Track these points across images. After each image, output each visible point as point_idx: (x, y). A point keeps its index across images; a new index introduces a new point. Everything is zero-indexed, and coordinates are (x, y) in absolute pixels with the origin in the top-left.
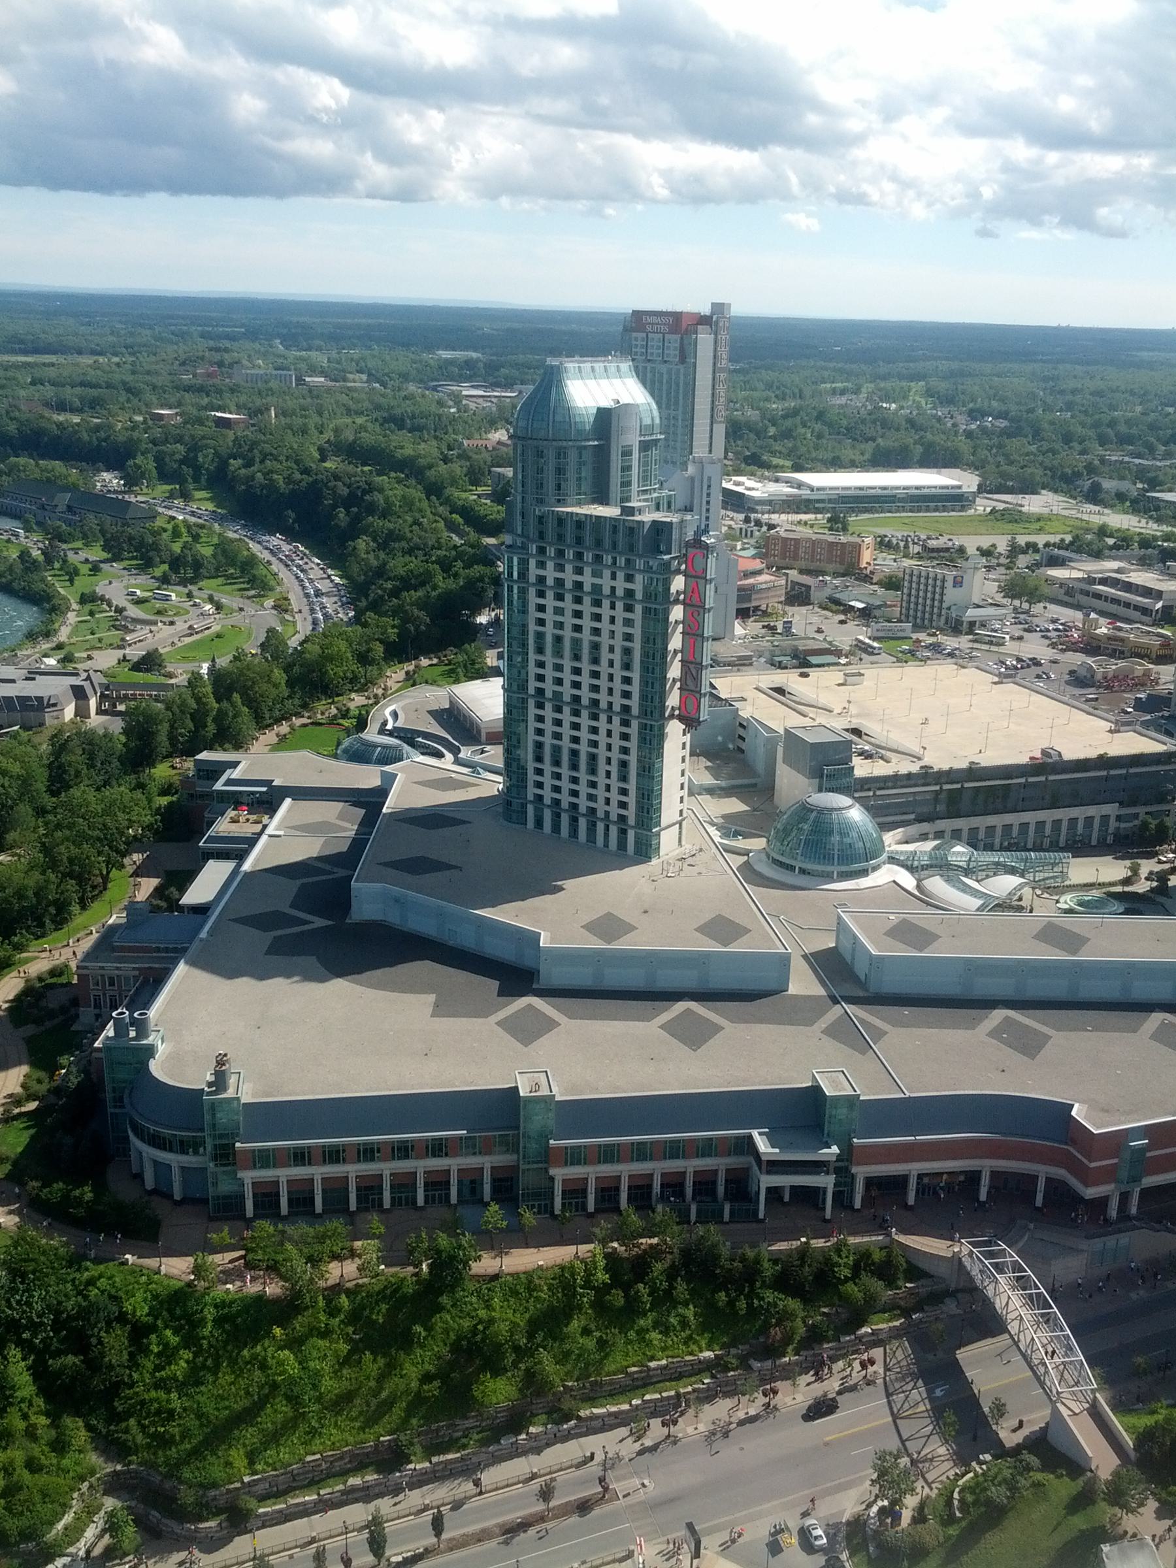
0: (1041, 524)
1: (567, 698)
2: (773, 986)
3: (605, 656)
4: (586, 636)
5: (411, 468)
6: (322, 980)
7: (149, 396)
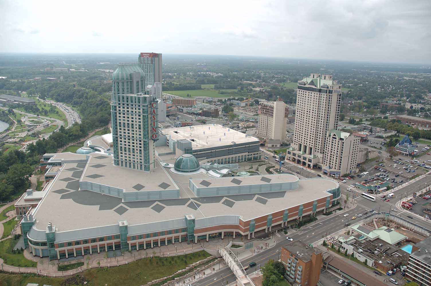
3: (135, 127)
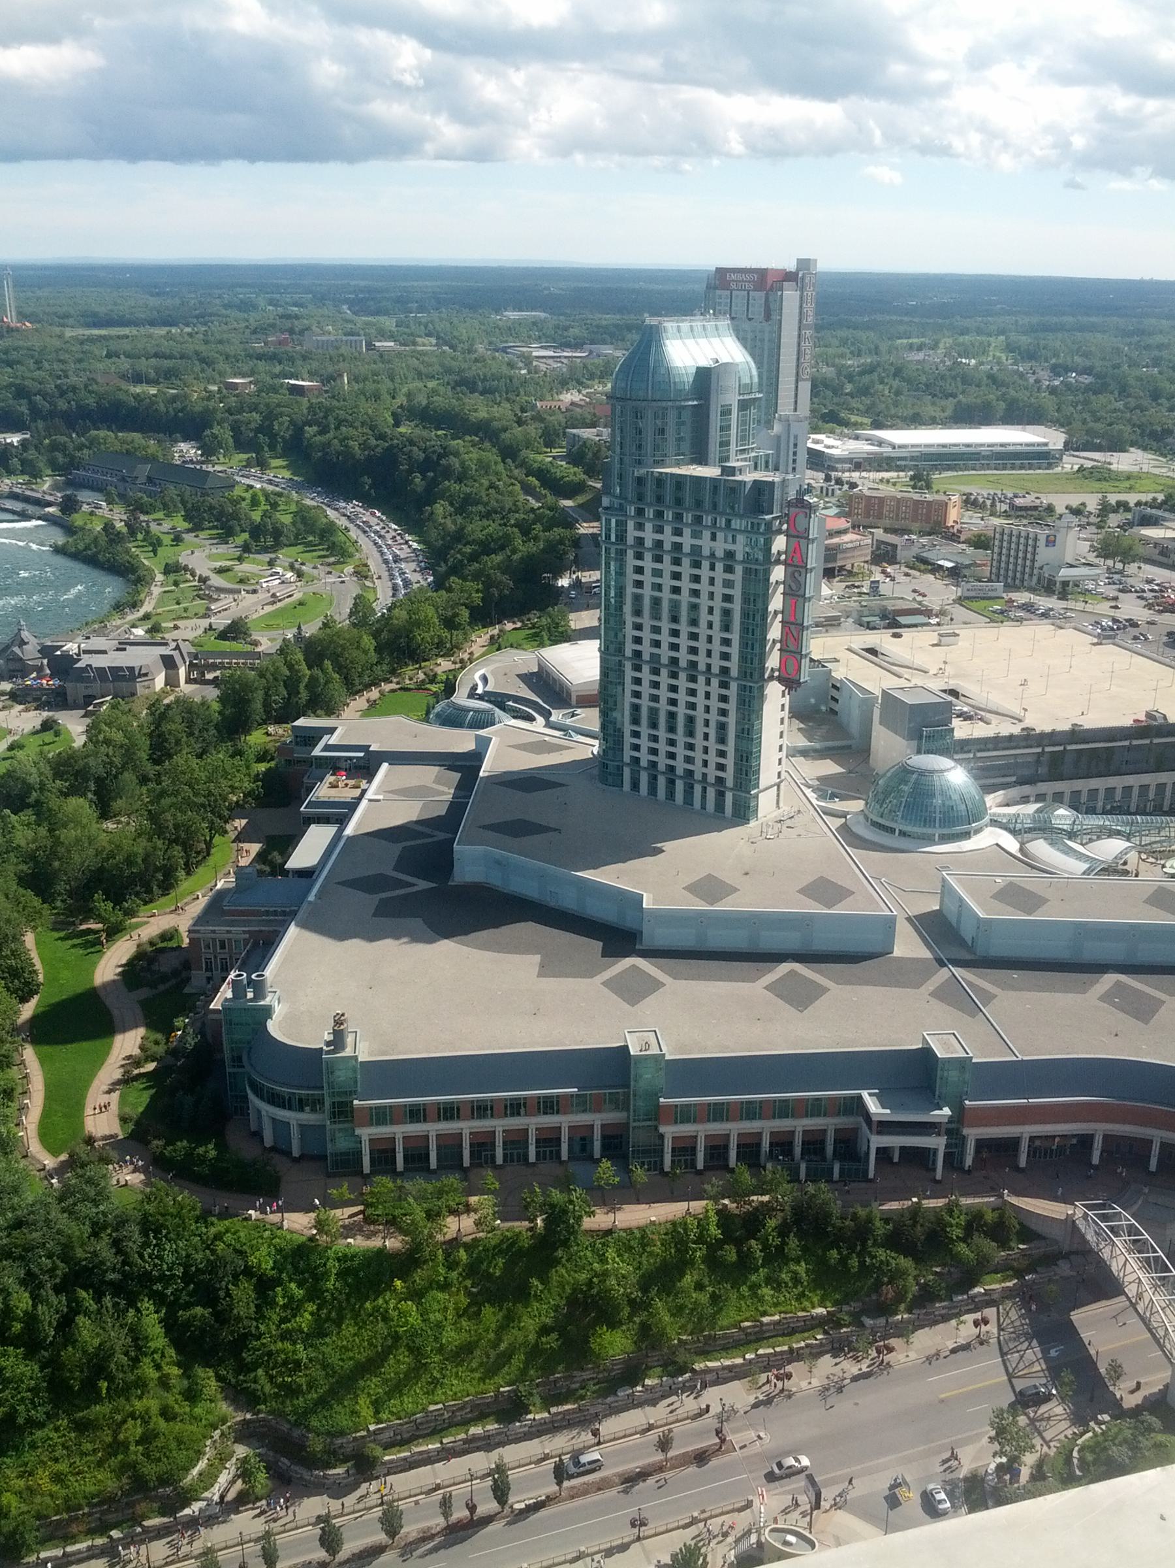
0: (1132, 482)
1: (664, 660)
2: (879, 949)
3: (704, 618)
4: (685, 598)
5: (485, 431)
6: (430, 941)
7: (222, 365)
